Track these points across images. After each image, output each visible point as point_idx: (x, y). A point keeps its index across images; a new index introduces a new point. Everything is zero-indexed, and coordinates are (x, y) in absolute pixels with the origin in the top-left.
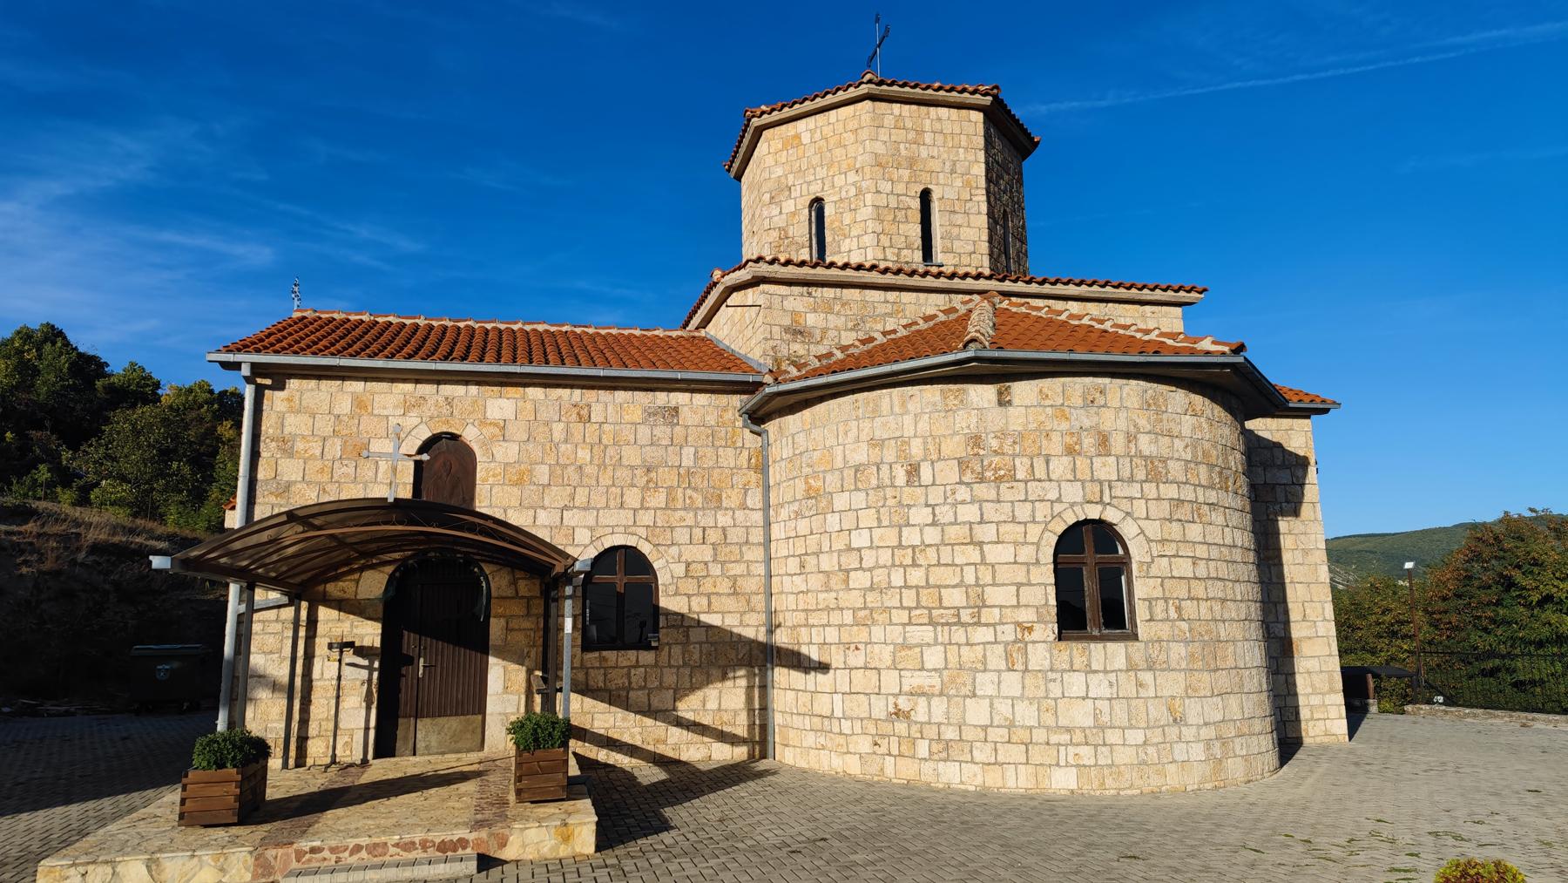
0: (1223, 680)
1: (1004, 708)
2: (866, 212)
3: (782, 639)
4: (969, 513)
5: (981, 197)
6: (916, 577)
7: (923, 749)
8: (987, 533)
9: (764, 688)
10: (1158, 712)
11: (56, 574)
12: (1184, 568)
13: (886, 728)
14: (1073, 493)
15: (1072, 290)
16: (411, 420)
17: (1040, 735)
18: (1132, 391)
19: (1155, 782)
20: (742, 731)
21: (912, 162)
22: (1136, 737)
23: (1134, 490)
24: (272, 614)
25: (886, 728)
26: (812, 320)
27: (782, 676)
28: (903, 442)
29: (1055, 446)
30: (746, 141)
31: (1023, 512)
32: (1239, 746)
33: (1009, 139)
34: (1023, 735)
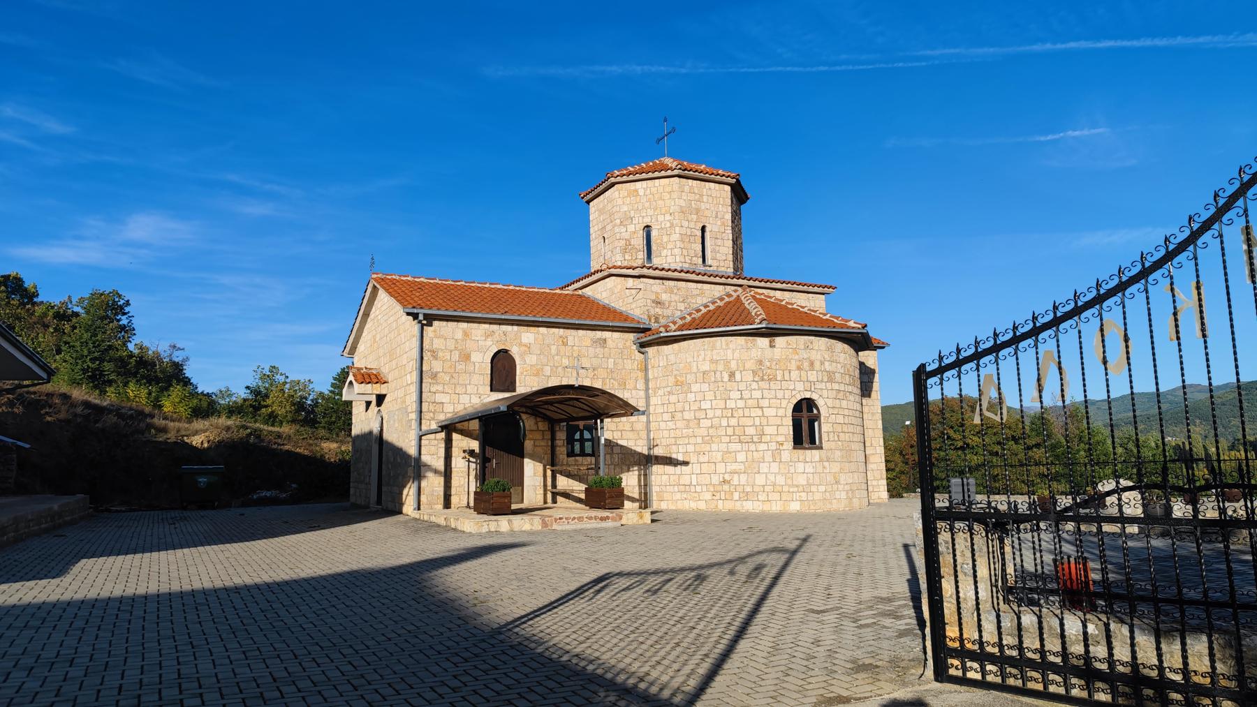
0: (853, 467)
1: (772, 478)
2: (675, 237)
3: (658, 451)
4: (757, 394)
5: (729, 231)
6: (733, 422)
7: (736, 496)
8: (765, 403)
9: (645, 475)
10: (830, 478)
11: (68, 421)
12: (840, 419)
13: (719, 488)
14: (800, 386)
15: (779, 286)
16: (489, 343)
17: (786, 489)
18: (823, 341)
19: (829, 506)
20: (636, 496)
21: (698, 211)
22: (822, 488)
23: (823, 386)
24: (432, 436)
25: (719, 488)
26: (664, 297)
27: (656, 469)
28: (727, 362)
29: (793, 366)
30: (602, 187)
31: (780, 394)
32: (857, 494)
33: (739, 195)
34: (779, 489)
